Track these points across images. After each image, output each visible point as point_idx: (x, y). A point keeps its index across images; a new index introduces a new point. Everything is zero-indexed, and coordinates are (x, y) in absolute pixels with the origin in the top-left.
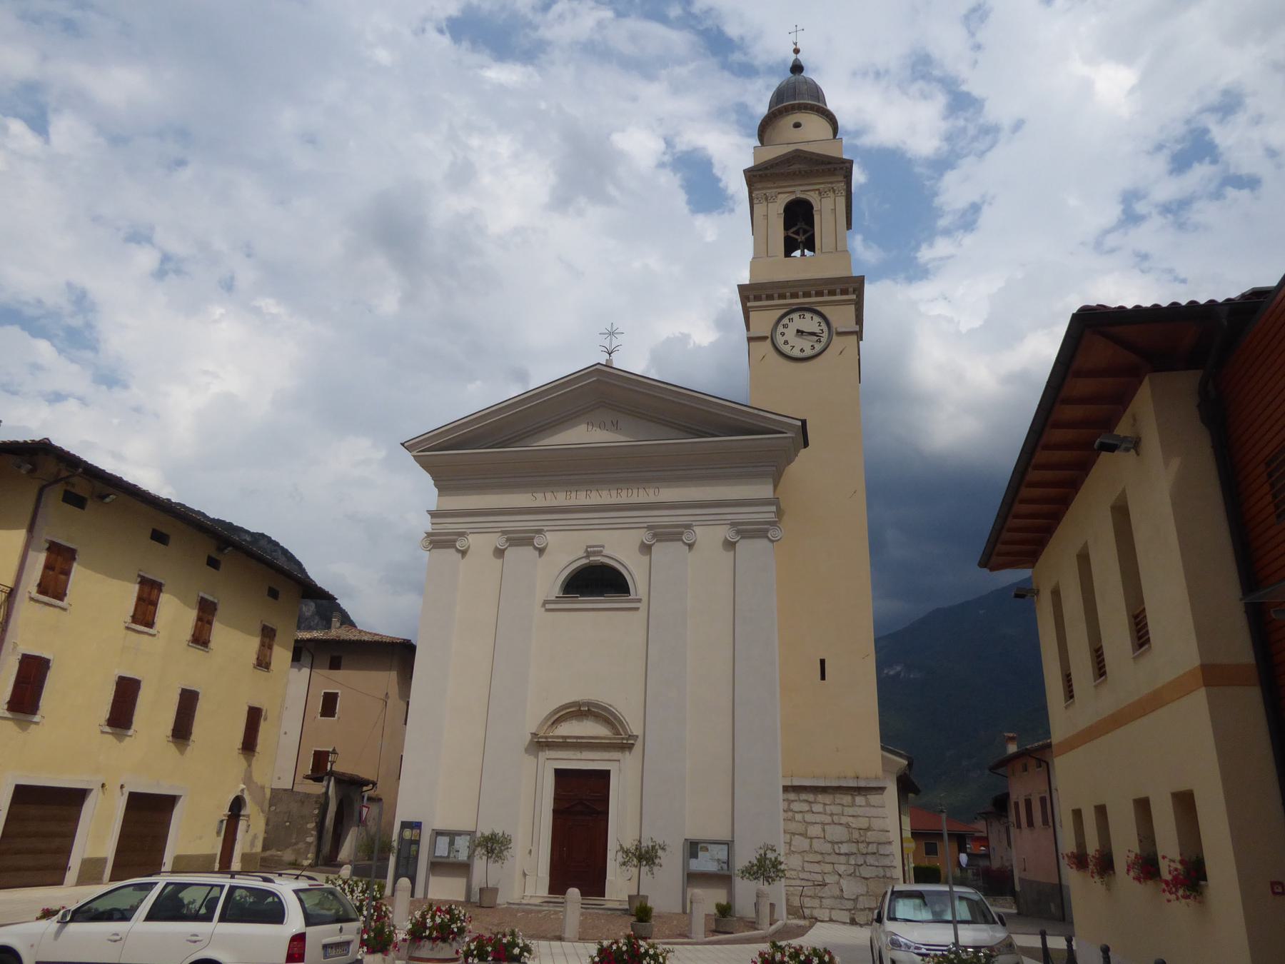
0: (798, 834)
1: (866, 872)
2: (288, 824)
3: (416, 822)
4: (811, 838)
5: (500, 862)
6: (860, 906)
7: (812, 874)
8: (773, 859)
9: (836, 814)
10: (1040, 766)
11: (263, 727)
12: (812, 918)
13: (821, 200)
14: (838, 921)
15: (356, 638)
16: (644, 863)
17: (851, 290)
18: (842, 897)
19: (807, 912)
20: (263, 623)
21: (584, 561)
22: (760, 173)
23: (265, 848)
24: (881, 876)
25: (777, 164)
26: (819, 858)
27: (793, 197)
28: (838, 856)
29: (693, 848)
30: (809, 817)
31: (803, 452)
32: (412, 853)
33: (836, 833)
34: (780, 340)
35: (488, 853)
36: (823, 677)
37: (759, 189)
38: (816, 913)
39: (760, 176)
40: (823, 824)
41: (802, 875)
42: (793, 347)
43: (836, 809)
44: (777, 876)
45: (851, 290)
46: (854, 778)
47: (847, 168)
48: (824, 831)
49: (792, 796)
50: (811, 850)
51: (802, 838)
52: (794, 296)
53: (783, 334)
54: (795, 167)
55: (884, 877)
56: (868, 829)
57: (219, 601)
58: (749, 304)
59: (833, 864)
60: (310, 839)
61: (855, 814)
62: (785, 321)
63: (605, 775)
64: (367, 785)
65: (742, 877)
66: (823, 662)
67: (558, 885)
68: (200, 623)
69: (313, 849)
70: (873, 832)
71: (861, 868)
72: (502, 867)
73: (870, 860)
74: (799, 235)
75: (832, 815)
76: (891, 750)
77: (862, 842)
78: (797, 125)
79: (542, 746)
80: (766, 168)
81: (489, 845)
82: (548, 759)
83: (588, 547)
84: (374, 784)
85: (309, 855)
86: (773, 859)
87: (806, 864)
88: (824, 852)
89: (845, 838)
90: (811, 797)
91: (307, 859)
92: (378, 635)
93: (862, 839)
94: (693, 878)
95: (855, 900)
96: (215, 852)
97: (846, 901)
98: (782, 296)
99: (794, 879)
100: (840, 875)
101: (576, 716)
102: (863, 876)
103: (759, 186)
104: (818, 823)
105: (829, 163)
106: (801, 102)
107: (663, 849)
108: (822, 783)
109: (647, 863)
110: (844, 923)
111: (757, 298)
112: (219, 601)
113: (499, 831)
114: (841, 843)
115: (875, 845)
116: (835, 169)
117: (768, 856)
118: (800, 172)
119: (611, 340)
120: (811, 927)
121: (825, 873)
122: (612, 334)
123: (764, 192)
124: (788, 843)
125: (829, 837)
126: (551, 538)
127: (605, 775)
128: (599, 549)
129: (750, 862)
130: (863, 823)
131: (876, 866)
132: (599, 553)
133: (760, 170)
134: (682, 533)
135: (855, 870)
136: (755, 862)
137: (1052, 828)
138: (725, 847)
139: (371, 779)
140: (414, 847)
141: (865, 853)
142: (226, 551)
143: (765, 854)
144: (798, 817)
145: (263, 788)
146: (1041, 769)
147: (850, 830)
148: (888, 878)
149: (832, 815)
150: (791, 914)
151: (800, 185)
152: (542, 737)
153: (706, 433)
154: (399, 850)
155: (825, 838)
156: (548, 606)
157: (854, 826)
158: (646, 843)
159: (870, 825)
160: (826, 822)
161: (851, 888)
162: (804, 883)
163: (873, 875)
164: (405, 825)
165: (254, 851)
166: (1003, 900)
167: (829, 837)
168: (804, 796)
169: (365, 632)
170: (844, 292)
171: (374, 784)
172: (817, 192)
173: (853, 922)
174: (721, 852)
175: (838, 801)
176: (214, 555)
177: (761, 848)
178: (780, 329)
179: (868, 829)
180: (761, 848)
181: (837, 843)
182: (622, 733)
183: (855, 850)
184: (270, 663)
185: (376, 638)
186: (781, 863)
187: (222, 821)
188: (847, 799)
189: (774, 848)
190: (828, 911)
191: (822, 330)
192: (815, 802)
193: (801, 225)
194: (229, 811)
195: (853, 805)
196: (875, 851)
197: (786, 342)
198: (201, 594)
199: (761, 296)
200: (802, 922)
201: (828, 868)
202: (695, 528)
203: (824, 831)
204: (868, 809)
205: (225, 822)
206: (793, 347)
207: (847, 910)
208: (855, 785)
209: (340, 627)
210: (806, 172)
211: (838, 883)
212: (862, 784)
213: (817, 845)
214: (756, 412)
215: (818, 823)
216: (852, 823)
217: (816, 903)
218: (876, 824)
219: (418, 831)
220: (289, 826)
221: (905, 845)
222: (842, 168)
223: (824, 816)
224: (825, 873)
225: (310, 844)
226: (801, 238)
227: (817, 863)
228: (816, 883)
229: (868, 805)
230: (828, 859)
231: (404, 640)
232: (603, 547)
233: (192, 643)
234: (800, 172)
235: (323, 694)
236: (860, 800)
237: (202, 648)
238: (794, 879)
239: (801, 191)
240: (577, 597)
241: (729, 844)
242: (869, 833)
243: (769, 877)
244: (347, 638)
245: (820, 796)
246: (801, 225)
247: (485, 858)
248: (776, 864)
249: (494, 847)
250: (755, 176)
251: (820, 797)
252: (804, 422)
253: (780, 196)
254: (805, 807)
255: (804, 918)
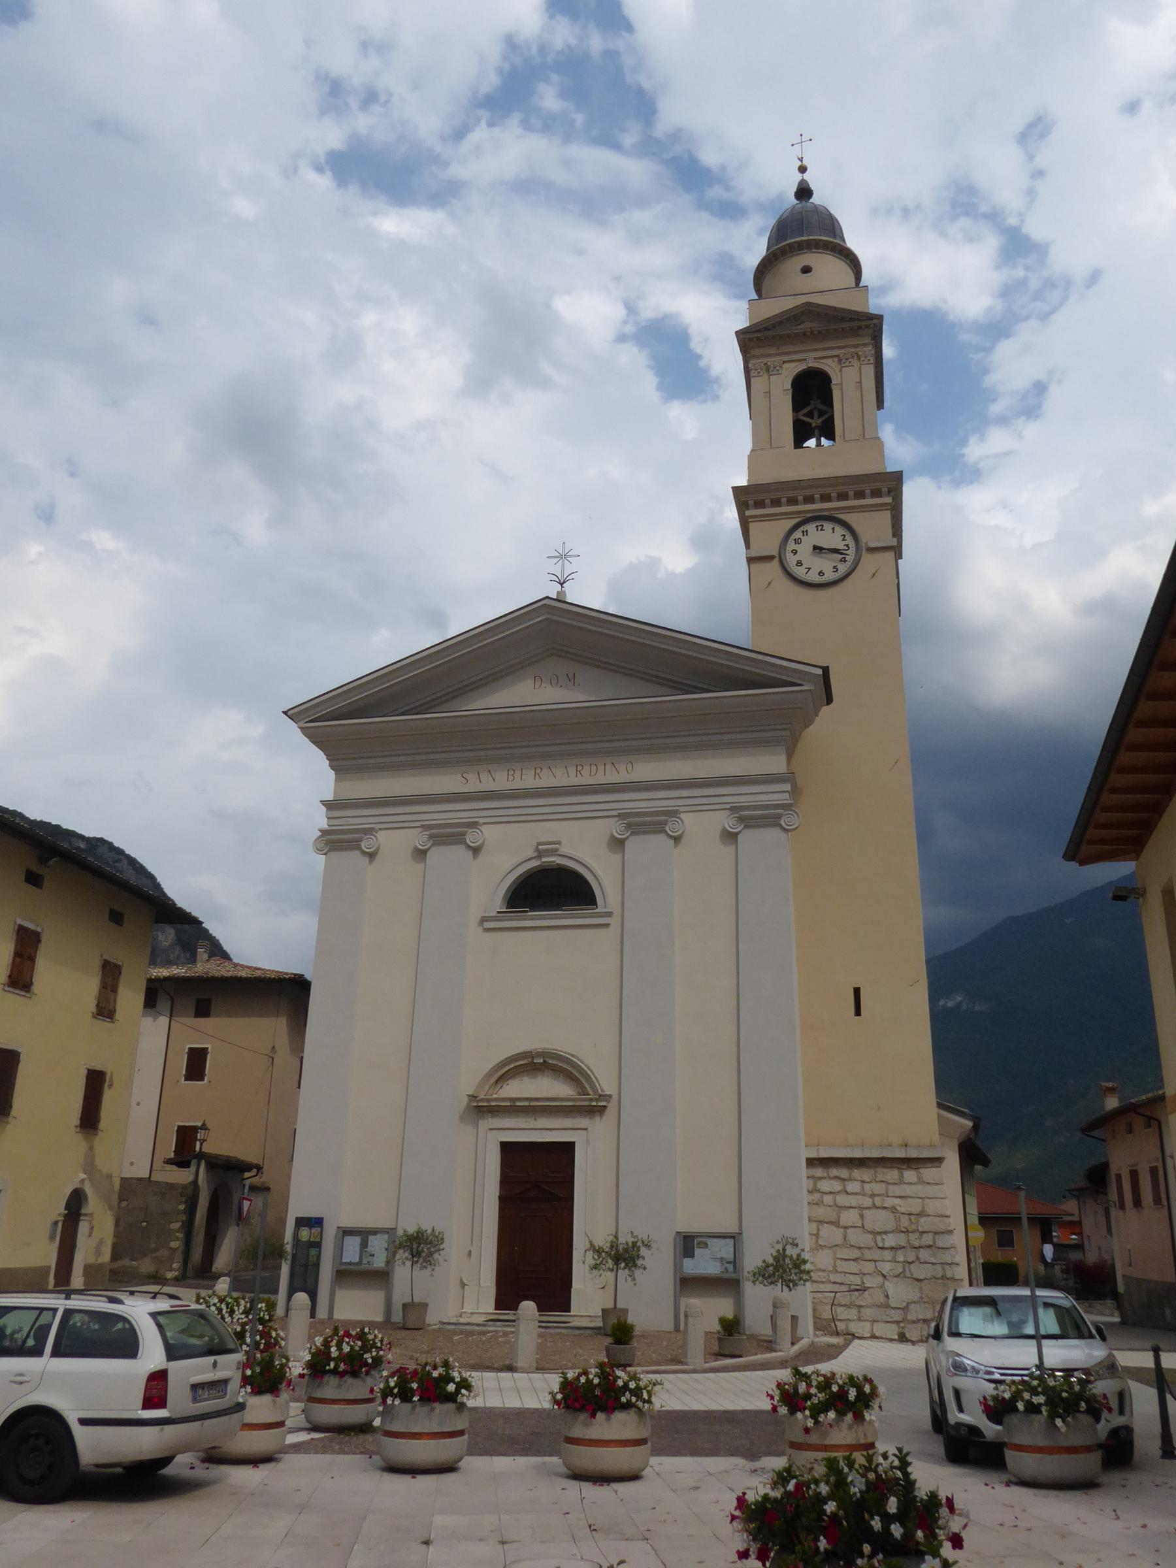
0: (827, 1223)
1: (919, 1271)
2: (144, 1224)
3: (316, 1218)
4: (845, 1228)
5: (430, 1268)
6: (911, 1316)
7: (847, 1275)
8: (795, 1257)
9: (879, 1195)
10: (1150, 1126)
11: (108, 1096)
12: (849, 1334)
13: (841, 370)
14: (882, 1338)
15: (229, 974)
16: (623, 1265)
17: (885, 490)
18: (887, 1306)
19: (841, 1326)
20: (105, 957)
21: (535, 863)
22: (759, 335)
23: (115, 1257)
24: (937, 1276)
25: (781, 323)
26: (856, 1253)
27: (802, 367)
28: (881, 1251)
29: (688, 1244)
30: (842, 1200)
31: (825, 710)
32: (311, 1259)
33: (882, 1220)
34: (791, 560)
35: (413, 1257)
36: (858, 1012)
37: (758, 357)
38: (854, 1327)
39: (758, 338)
40: (861, 1208)
41: (833, 1277)
42: (810, 569)
43: (878, 1188)
44: (801, 1279)
45: (885, 490)
46: (902, 1146)
47: (875, 325)
48: (862, 1216)
49: (819, 1172)
50: (846, 1244)
51: (834, 1228)
52: (809, 500)
53: (795, 552)
54: (807, 326)
55: (943, 1277)
56: (921, 1214)
57: (43, 929)
58: (748, 513)
59: (875, 1261)
60: (174, 1244)
61: (903, 1194)
62: (798, 534)
63: (569, 1148)
64: (249, 1170)
65: (754, 1282)
66: (857, 991)
67: (507, 1298)
68: (18, 960)
69: (179, 1256)
70: (929, 1218)
71: (912, 1266)
72: (432, 1275)
73: (924, 1255)
74: (813, 418)
75: (872, 1196)
76: (950, 1107)
77: (913, 1232)
78: (806, 270)
79: (483, 1112)
80: (766, 329)
81: (415, 1246)
82: (490, 1129)
83: (539, 844)
84: (259, 1168)
85: (175, 1265)
86: (795, 1257)
87: (839, 1263)
88: (862, 1246)
89: (891, 1225)
90: (843, 1173)
91: (171, 1270)
92: (259, 969)
93: (914, 1227)
94: (688, 1284)
95: (905, 1309)
96: (49, 1264)
97: (893, 1311)
98: (792, 501)
99: (823, 1282)
100: (884, 1276)
101: (526, 1071)
102: (914, 1276)
103: (754, 352)
104: (855, 1208)
105: (851, 320)
106: (811, 238)
107: (648, 1246)
108: (858, 1154)
109: (627, 1265)
110: (891, 1340)
111: (759, 504)
112: (43, 929)
113: (427, 1227)
114: (886, 1233)
115: (930, 1236)
116: (860, 328)
117: (788, 1253)
118: (812, 332)
119: (563, 565)
120: (846, 1346)
121: (864, 1274)
122: (563, 557)
123: (765, 360)
124: (814, 1234)
125: (869, 1227)
126: (489, 834)
127: (569, 1148)
128: (554, 846)
129: (764, 1261)
130: (914, 1206)
131: (933, 1264)
132: (554, 852)
133: (759, 331)
134: (779, 817)
135: (904, 1268)
136: (771, 1261)
137: (1165, 1211)
138: (731, 1242)
139: (255, 1161)
140: (313, 1252)
141: (917, 1245)
142: (51, 863)
143: (784, 1250)
144: (828, 1199)
145: (109, 1177)
146: (1151, 1130)
147: (897, 1215)
148: (948, 1279)
149: (872, 1196)
150: (819, 1330)
151: (816, 350)
152: (482, 1100)
153: (692, 686)
154: (294, 1256)
155: (863, 1227)
156: (488, 925)
157: (902, 1210)
158: (625, 1239)
159: (923, 1207)
160: (866, 1205)
161: (899, 1293)
162: (836, 1288)
163: (929, 1276)
164: (301, 1222)
165: (100, 1261)
166: (1101, 1304)
167: (869, 1227)
168: (834, 1172)
169: (242, 966)
170: (876, 493)
171: (259, 1168)
172: (836, 359)
173: (902, 1338)
174: (724, 1249)
175: (880, 1177)
176: (36, 868)
177: (778, 1242)
178: (791, 545)
179: (921, 1214)
180: (778, 1242)
181: (880, 1233)
182: (591, 1092)
183: (903, 1244)
184: (115, 1011)
185: (257, 974)
186: (805, 1262)
187: (56, 1223)
188: (892, 1174)
189: (796, 1242)
190: (869, 1324)
191: (847, 546)
192: (850, 1179)
193: (815, 404)
194: (65, 1209)
195: (901, 1182)
196: (931, 1243)
197: (799, 563)
198: (19, 921)
199: (797, 500)
200: (834, 1340)
201: (869, 1267)
202: (683, 816)
203: (862, 1216)
204: (919, 1187)
205: (60, 1224)
206: (810, 569)
207: (894, 1322)
208: (903, 1155)
209: (208, 960)
210: (820, 332)
211: (882, 1286)
212: (913, 1154)
213: (854, 1237)
214: (760, 657)
215: (855, 1208)
216: (900, 1206)
217: (853, 1313)
218: (932, 1206)
219: (319, 1230)
220: (147, 1226)
221: (970, 1234)
222: (867, 327)
223: (859, 1197)
224: (864, 1274)
225: (174, 1250)
226: (816, 422)
227: (853, 1260)
228: (852, 1287)
229: (921, 1181)
230: (868, 1255)
231: (295, 975)
232: (559, 843)
233: (9, 986)
234: (812, 332)
235: (187, 1050)
236: (910, 1175)
237: (23, 993)
238: (823, 1282)
239: (815, 358)
240: (527, 912)
241: (735, 1238)
242: (922, 1220)
243: (790, 1281)
244: (217, 974)
245: (856, 1171)
246: (815, 404)
247: (409, 1263)
248: (798, 1263)
249: (420, 1248)
250: (750, 339)
251: (857, 1173)
252: (826, 670)
253: (786, 366)
254: (837, 1186)
255: (838, 1334)
